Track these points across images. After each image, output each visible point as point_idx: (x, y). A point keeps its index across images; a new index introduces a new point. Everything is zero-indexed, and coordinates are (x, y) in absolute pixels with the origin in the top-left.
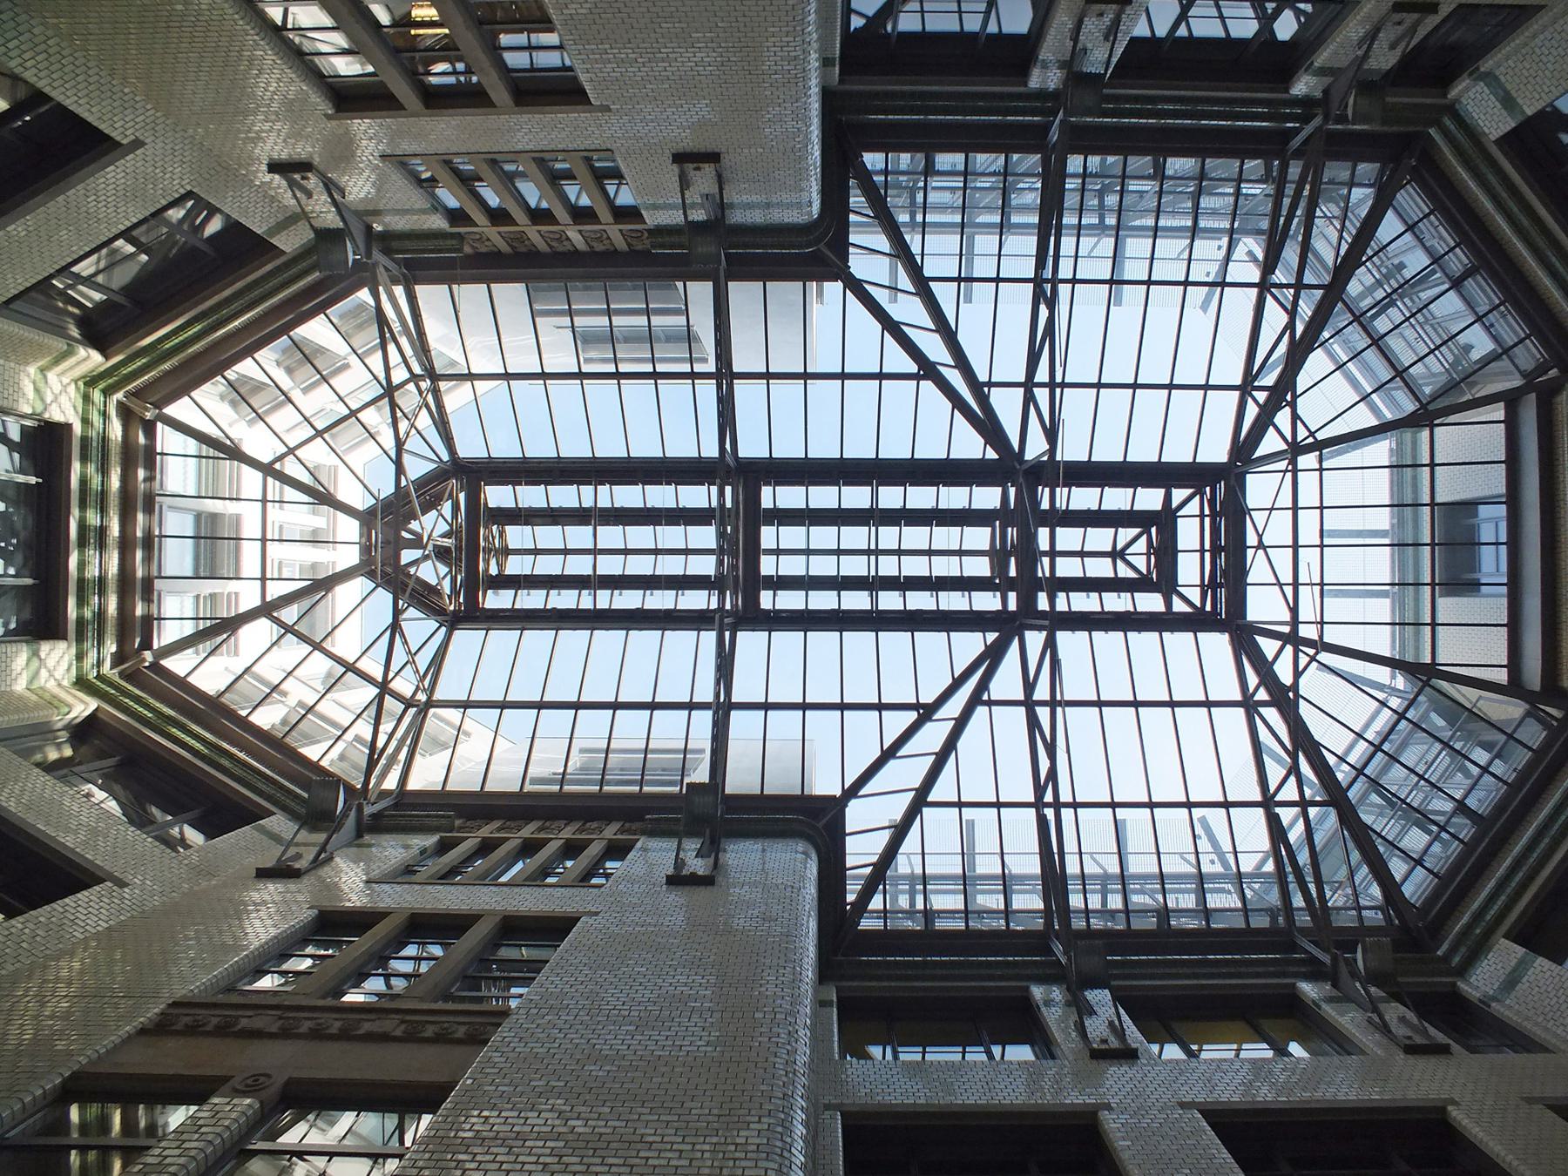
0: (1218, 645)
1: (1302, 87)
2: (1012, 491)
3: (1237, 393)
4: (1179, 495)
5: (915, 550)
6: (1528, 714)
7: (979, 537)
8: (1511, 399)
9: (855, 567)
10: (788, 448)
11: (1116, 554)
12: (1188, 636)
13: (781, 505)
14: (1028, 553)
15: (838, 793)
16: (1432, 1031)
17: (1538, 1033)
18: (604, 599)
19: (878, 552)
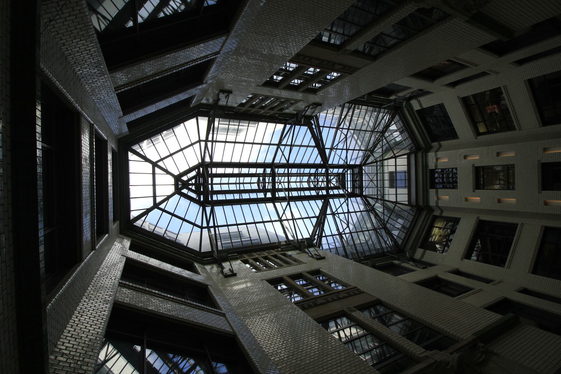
1: (393, 97)
5: (231, 184)
6: (411, 209)
8: (409, 155)
14: (205, 184)
15: (309, 237)
17: (434, 262)
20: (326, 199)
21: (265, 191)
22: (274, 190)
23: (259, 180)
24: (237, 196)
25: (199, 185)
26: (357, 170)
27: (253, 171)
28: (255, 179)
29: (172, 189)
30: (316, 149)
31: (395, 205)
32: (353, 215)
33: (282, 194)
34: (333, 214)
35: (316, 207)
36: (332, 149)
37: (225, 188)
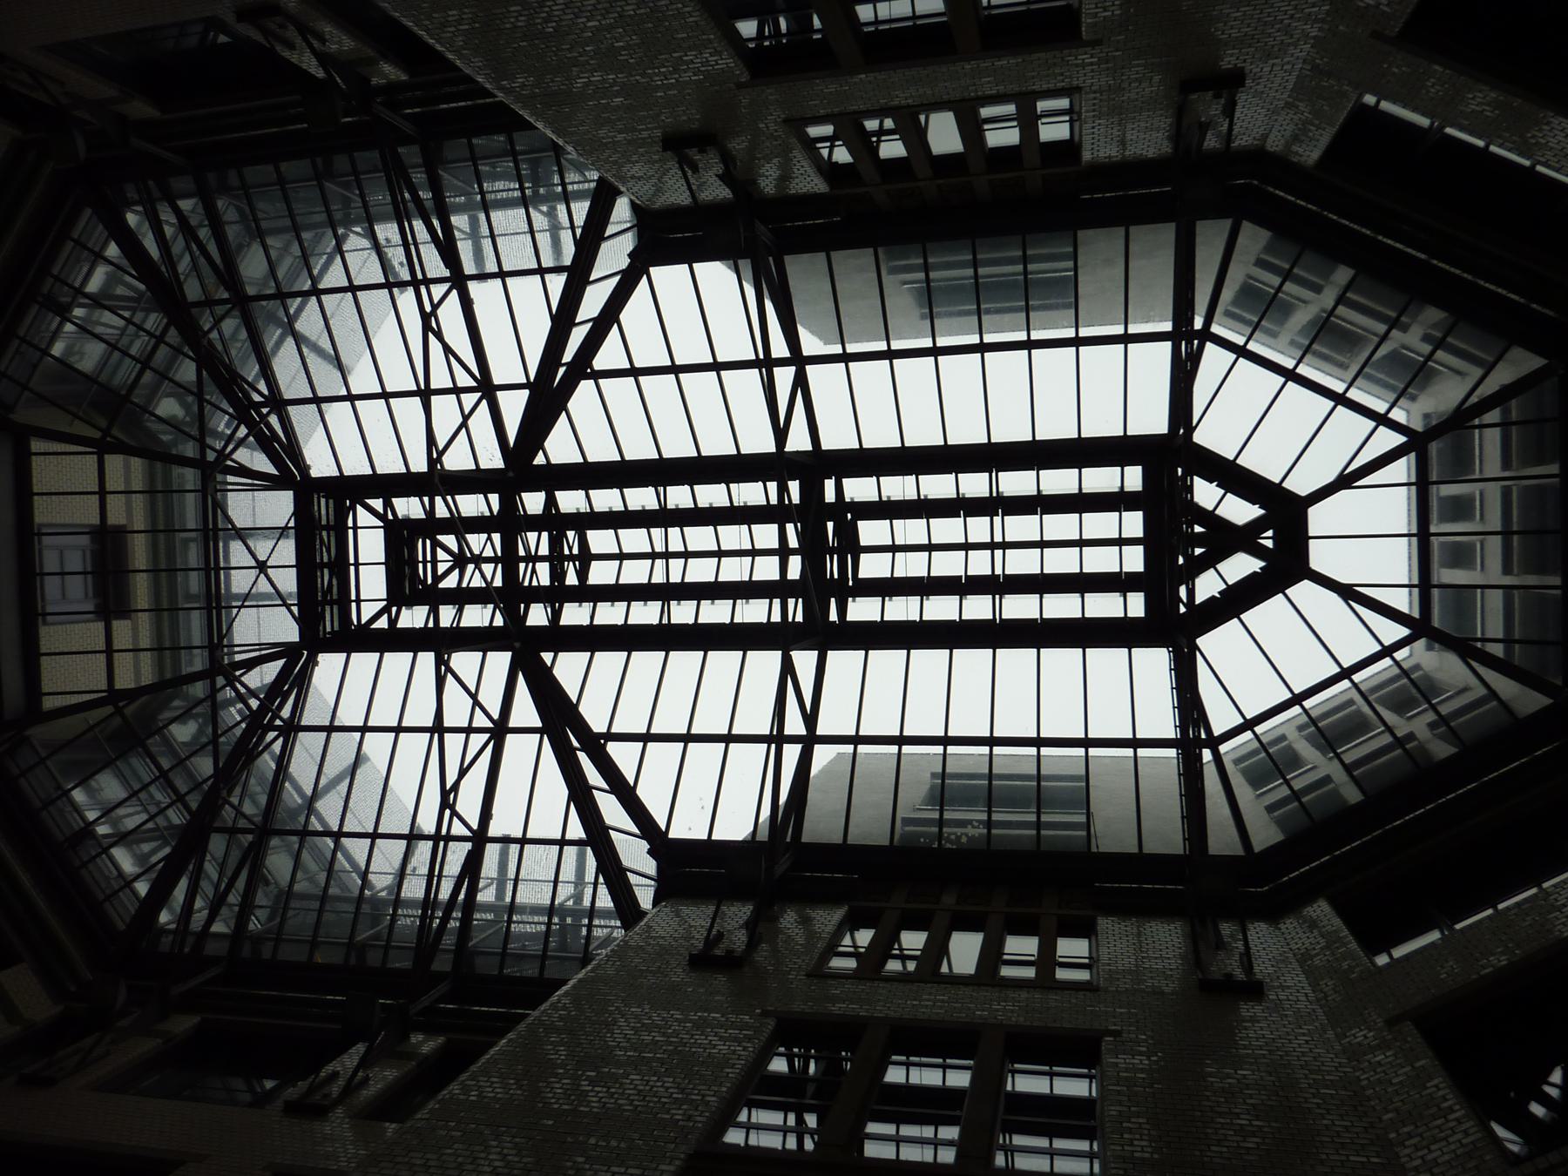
0: (320, 465)
1: (183, 1024)
2: (833, 617)
3: (512, 724)
4: (382, 623)
7: (872, 567)
9: (1021, 527)
10: (1107, 661)
11: (460, 561)
12: (668, 453)
13: (1076, 597)
14: (813, 549)
16: (257, 36)
18: (975, 484)
19: (991, 546)
20: (521, 466)
21: (553, 521)
22: (509, 523)
23: (582, 574)
24: (679, 497)
25: (1198, 539)
26: (327, 624)
27: (610, 614)
28: (601, 574)
29: (1319, 518)
30: (598, 725)
31: (106, 432)
32: (399, 379)
33: (472, 505)
34: (487, 388)
35: (586, 430)
36: (500, 731)
37: (733, 536)
